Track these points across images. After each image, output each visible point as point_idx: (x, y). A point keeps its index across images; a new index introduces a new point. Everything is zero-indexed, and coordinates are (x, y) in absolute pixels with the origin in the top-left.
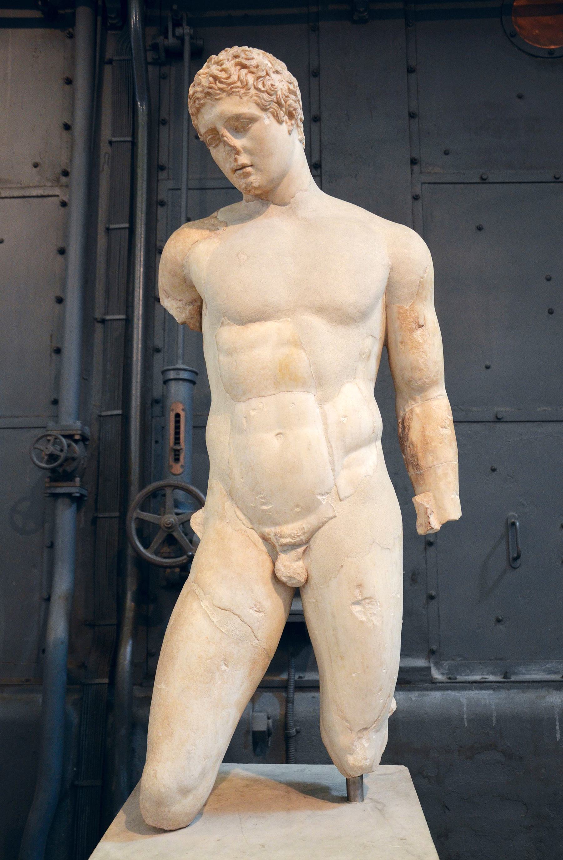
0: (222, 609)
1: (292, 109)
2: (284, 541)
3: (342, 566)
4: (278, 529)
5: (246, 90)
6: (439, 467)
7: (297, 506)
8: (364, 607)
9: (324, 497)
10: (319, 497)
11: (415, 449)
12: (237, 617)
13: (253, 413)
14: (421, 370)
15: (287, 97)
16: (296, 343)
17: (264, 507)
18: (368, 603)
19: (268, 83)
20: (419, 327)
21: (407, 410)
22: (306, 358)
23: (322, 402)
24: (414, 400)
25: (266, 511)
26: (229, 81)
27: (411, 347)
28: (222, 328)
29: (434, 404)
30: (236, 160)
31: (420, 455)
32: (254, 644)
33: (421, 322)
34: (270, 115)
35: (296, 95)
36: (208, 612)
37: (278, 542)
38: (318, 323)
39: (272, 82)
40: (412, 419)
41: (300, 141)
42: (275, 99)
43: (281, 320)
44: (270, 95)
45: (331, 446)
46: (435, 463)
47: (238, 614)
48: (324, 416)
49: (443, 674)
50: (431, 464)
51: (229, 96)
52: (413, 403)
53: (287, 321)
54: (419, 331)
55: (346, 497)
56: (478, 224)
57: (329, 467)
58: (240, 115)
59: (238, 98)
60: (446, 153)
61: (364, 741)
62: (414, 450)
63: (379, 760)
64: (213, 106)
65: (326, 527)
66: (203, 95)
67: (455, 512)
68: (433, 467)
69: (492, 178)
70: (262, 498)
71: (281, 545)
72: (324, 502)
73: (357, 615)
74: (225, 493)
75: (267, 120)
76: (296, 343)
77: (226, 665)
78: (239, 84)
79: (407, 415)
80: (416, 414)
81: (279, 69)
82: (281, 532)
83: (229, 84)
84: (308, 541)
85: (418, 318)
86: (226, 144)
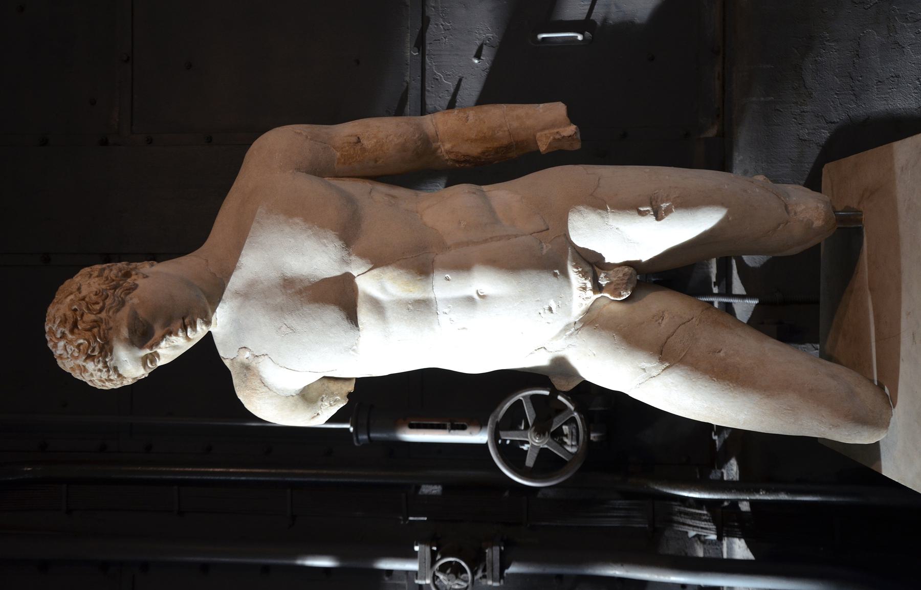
1: (120, 274)
15: (107, 279)
29: (441, 128)
31: (496, 144)
33: (354, 139)
34: (128, 298)
35: (104, 269)
39: (92, 295)
41: (152, 265)
42: (112, 291)
44: (107, 296)
46: (506, 129)
48: (459, 245)
50: (507, 133)
52: (439, 151)
54: (365, 143)
59: (111, 332)
61: (799, 209)
63: (883, 448)
67: (558, 110)
75: (133, 300)
78: (96, 330)
79: (452, 157)
80: (452, 147)
81: (75, 287)
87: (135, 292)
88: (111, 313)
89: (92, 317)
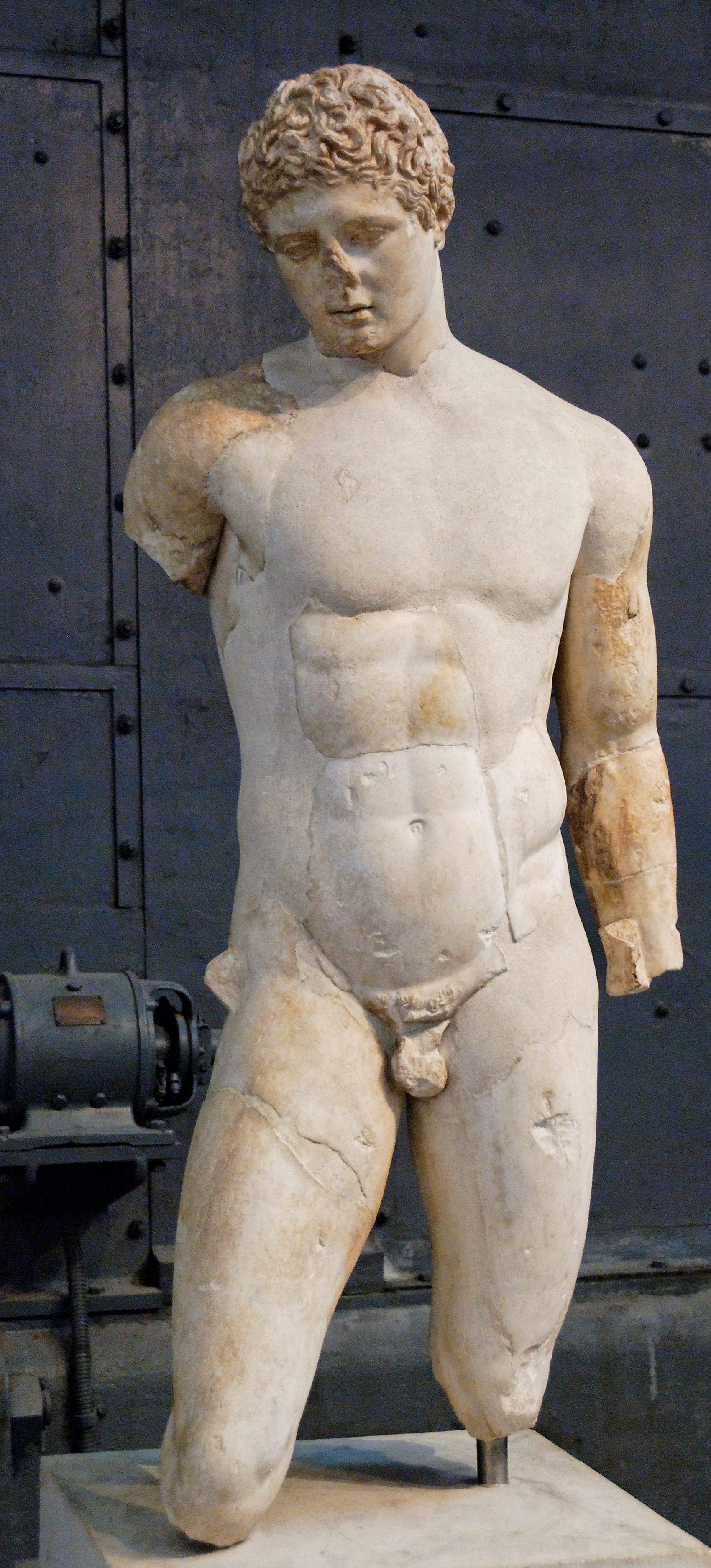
0: (314, 1142)
2: (416, 1015)
3: (519, 1060)
4: (404, 994)
5: (385, 174)
6: (650, 875)
7: (445, 952)
8: (553, 1130)
9: (488, 936)
10: (482, 936)
11: (608, 840)
12: (336, 1154)
13: (366, 781)
14: (626, 696)
16: (449, 656)
17: (382, 955)
18: (560, 1124)
19: (421, 160)
20: (629, 618)
21: (590, 766)
22: (467, 685)
23: (488, 762)
24: (606, 748)
25: (382, 962)
26: (356, 156)
27: (613, 653)
28: (304, 617)
30: (346, 296)
31: (617, 850)
32: (359, 1203)
33: (634, 609)
34: (415, 217)
36: (291, 1147)
37: (402, 1015)
38: (474, 610)
40: (600, 784)
43: (419, 609)
44: (422, 182)
45: (504, 844)
47: (339, 1148)
48: (491, 789)
49: (402, 1269)
51: (354, 182)
52: (603, 753)
53: (431, 611)
55: (524, 936)
56: (489, 219)
57: (500, 884)
58: (371, 219)
59: (368, 187)
60: (420, 32)
62: (604, 841)
64: (318, 194)
65: (488, 988)
66: (302, 171)
67: (672, 956)
68: (641, 875)
69: (521, 107)
70: (379, 937)
71: (406, 1023)
72: (488, 945)
73: (542, 1145)
74: (294, 924)
75: (411, 226)
76: (449, 656)
77: (321, 1242)
78: (373, 162)
79: (592, 775)
80: (611, 776)
82: (411, 999)
83: (359, 161)
84: (453, 1016)
85: (629, 602)
86: (329, 263)
87: (420, 228)
88: (399, 189)
89: (394, 160)
